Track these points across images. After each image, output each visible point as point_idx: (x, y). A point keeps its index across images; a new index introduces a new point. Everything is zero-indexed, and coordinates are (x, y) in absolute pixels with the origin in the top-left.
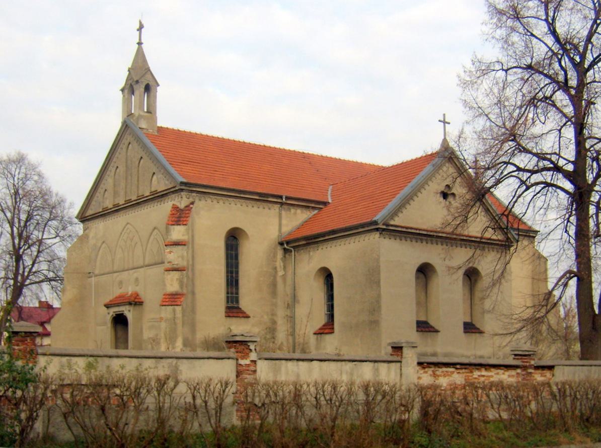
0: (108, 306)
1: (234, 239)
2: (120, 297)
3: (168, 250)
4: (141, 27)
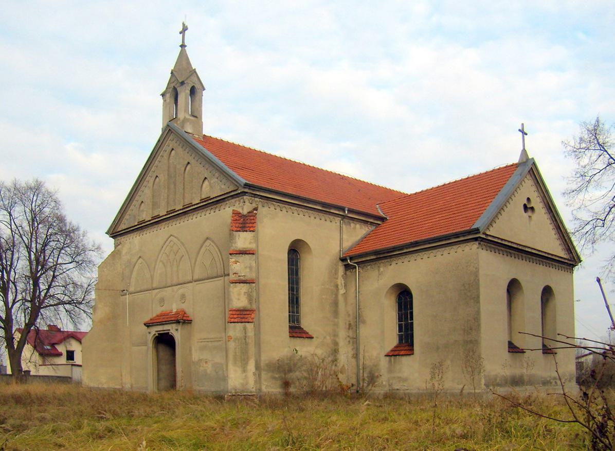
0: (148, 325)
1: (295, 251)
2: (162, 315)
3: (233, 260)
4: (185, 29)
